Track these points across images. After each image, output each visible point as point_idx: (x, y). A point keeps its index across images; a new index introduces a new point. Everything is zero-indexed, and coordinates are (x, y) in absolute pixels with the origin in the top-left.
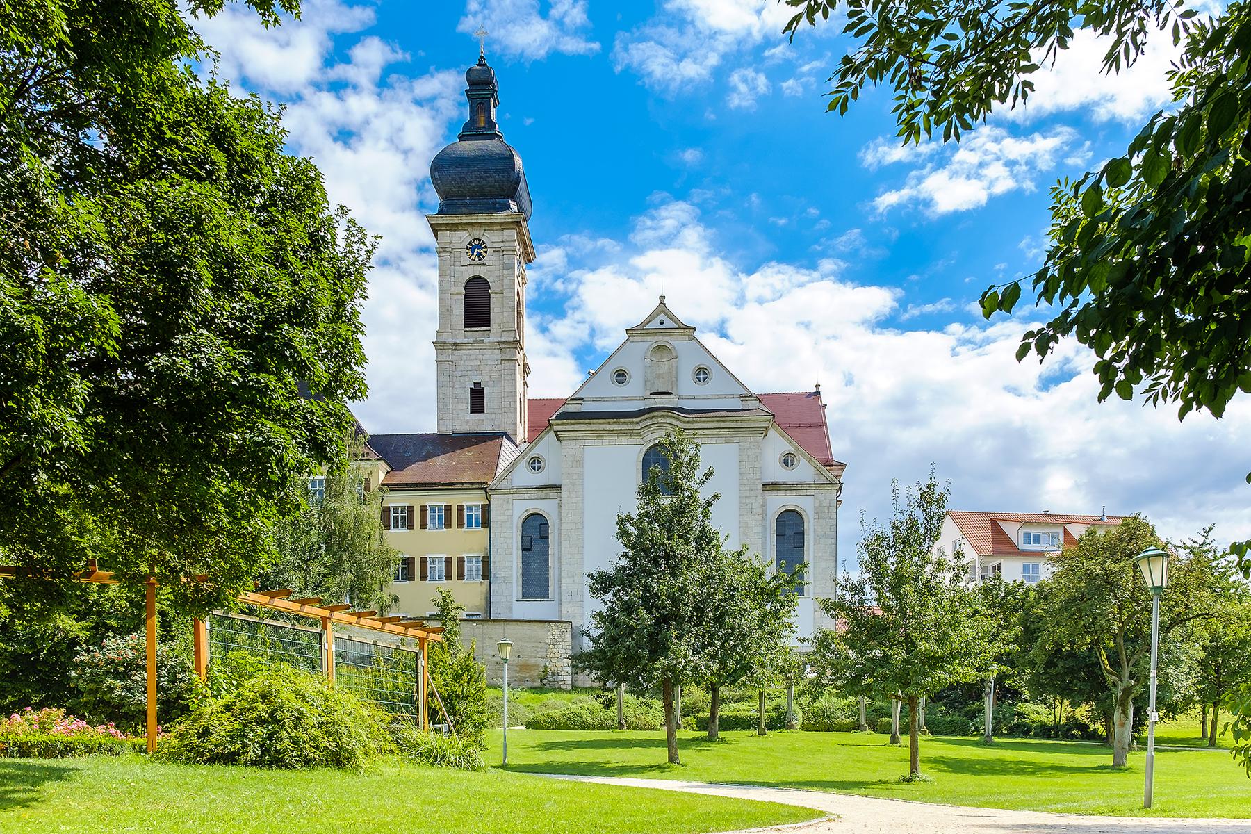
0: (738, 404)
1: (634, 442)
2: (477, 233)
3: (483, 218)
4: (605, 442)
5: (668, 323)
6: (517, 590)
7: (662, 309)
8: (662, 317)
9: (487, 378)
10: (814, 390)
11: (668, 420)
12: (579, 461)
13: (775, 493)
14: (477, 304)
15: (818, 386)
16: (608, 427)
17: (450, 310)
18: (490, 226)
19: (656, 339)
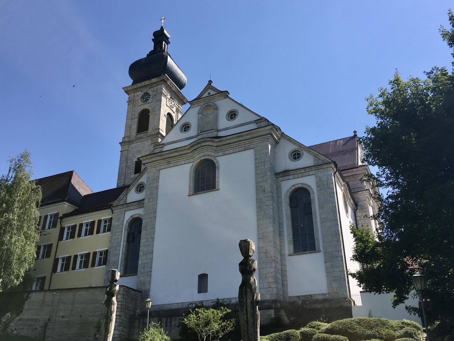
1: (188, 161)
2: (145, 90)
3: (147, 82)
4: (172, 165)
6: (288, 247)
7: (210, 85)
8: (210, 91)
10: (352, 135)
11: (207, 144)
13: (287, 178)
17: (130, 127)
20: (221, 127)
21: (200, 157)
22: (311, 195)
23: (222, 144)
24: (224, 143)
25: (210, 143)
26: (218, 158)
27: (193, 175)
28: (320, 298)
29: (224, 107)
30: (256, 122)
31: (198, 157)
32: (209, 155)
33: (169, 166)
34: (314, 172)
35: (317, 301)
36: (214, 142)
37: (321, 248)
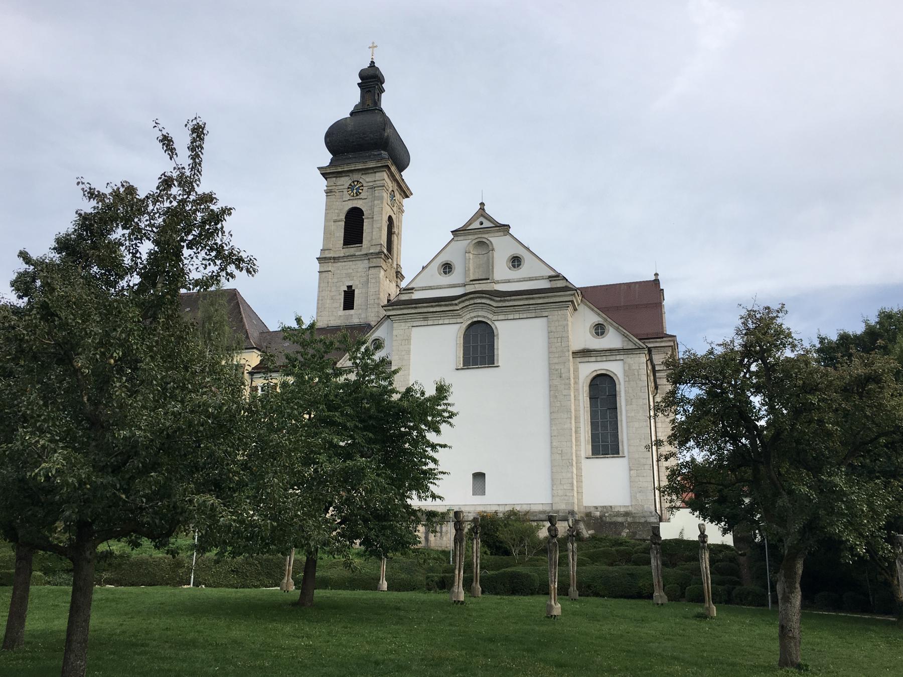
0: (545, 284)
1: (454, 321)
2: (356, 176)
4: (430, 322)
5: (487, 224)
6: (586, 447)
7: (482, 212)
8: (482, 219)
9: (357, 283)
10: (653, 278)
11: (484, 301)
12: (408, 340)
13: (587, 359)
14: (353, 226)
15: (656, 275)
16: (431, 310)
18: (365, 171)
19: (476, 236)
20: (497, 276)
21: (472, 318)
22: (617, 386)
23: (504, 304)
24: (507, 304)
25: (488, 302)
26: (496, 323)
27: (461, 341)
28: (622, 510)
29: (502, 248)
30: (551, 278)
31: (468, 316)
32: (484, 317)
33: (425, 323)
34: (622, 357)
35: (618, 514)
36: (494, 300)
37: (626, 454)
